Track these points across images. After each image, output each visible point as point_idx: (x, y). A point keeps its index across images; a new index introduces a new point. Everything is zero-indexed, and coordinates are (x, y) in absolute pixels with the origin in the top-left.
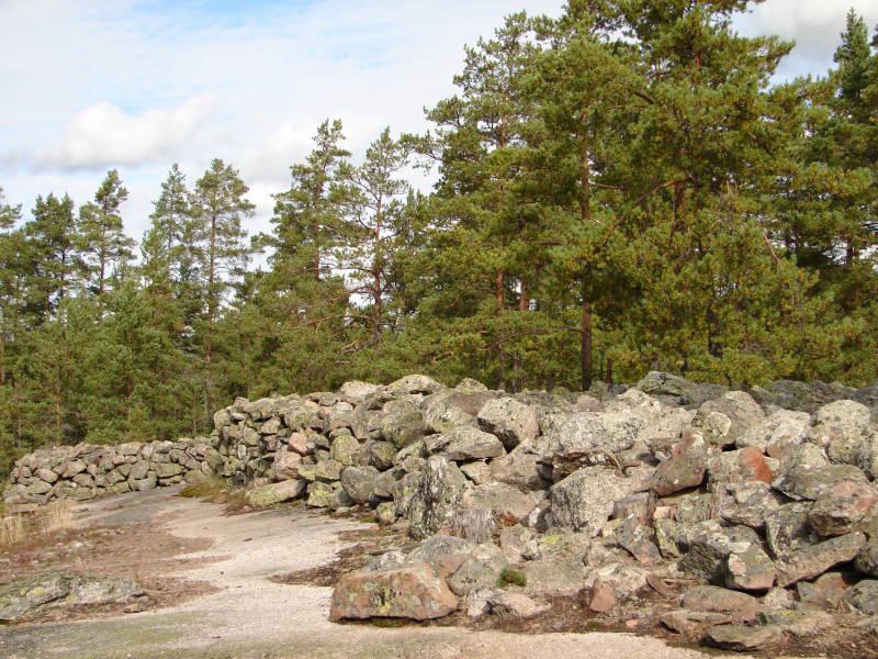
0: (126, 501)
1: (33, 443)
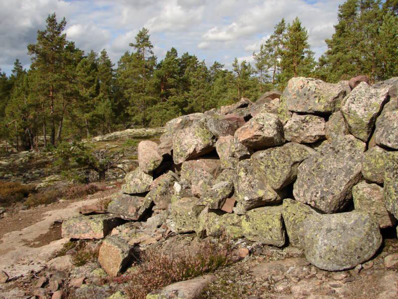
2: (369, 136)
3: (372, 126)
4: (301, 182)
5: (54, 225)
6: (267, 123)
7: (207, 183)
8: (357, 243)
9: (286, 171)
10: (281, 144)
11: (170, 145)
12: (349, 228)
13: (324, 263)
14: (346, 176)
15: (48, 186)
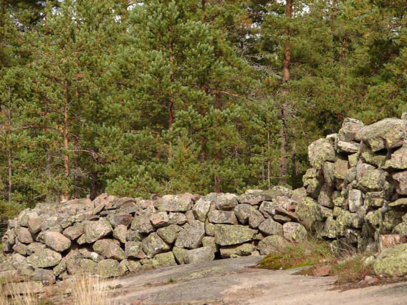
0: (178, 274)
1: (32, 198)
3: (207, 217)
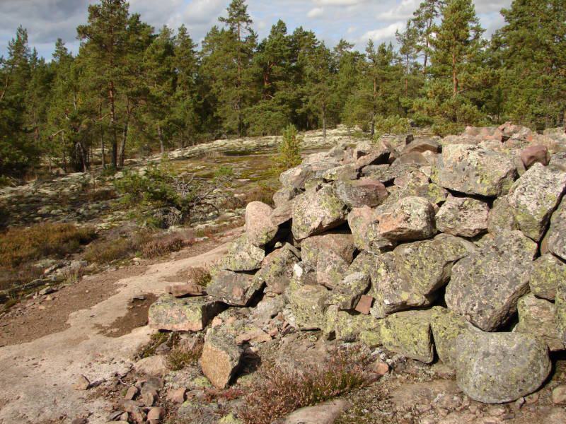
2: (541, 235)
3: (546, 224)
4: (455, 286)
5: (133, 302)
6: (414, 211)
7: (336, 270)
8: (519, 374)
9: (437, 273)
10: (432, 236)
11: (288, 213)
12: (510, 355)
13: (479, 394)
14: (510, 286)
15: (112, 228)
